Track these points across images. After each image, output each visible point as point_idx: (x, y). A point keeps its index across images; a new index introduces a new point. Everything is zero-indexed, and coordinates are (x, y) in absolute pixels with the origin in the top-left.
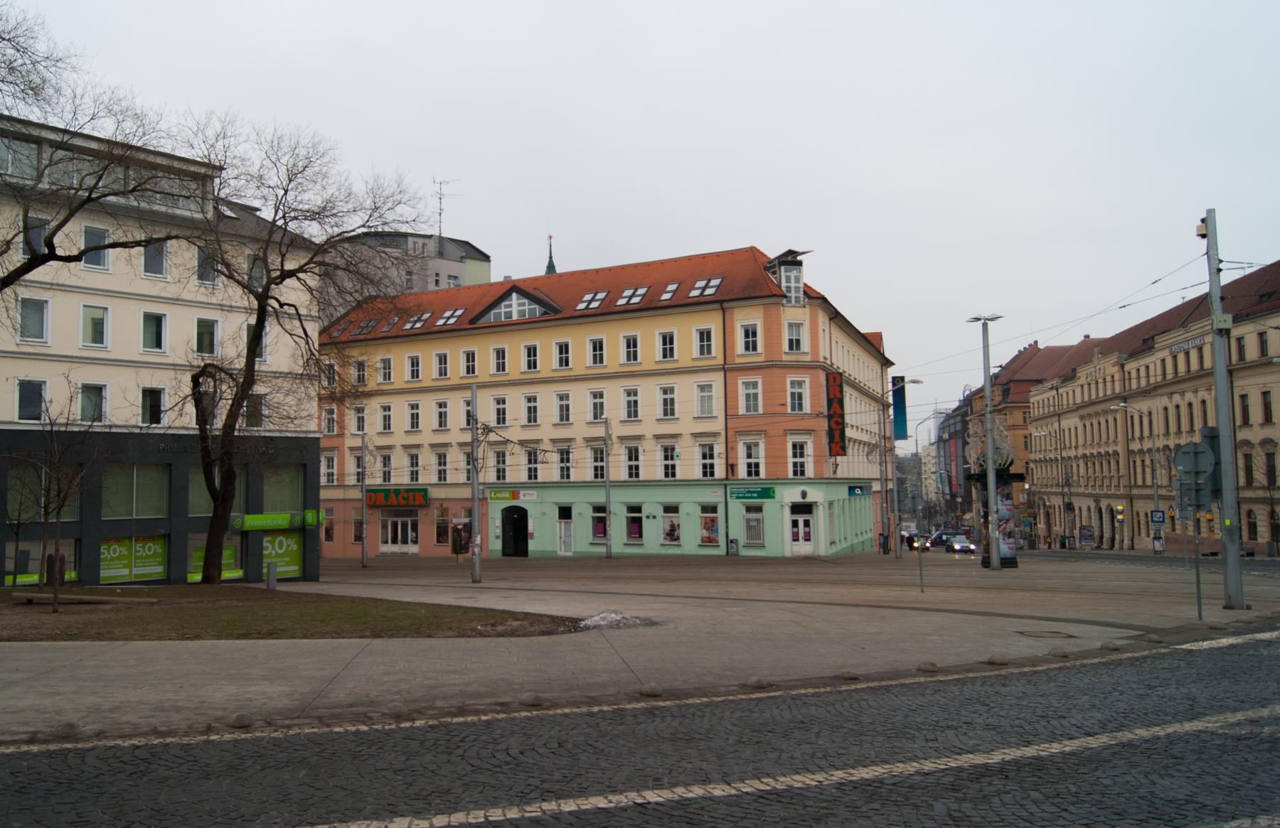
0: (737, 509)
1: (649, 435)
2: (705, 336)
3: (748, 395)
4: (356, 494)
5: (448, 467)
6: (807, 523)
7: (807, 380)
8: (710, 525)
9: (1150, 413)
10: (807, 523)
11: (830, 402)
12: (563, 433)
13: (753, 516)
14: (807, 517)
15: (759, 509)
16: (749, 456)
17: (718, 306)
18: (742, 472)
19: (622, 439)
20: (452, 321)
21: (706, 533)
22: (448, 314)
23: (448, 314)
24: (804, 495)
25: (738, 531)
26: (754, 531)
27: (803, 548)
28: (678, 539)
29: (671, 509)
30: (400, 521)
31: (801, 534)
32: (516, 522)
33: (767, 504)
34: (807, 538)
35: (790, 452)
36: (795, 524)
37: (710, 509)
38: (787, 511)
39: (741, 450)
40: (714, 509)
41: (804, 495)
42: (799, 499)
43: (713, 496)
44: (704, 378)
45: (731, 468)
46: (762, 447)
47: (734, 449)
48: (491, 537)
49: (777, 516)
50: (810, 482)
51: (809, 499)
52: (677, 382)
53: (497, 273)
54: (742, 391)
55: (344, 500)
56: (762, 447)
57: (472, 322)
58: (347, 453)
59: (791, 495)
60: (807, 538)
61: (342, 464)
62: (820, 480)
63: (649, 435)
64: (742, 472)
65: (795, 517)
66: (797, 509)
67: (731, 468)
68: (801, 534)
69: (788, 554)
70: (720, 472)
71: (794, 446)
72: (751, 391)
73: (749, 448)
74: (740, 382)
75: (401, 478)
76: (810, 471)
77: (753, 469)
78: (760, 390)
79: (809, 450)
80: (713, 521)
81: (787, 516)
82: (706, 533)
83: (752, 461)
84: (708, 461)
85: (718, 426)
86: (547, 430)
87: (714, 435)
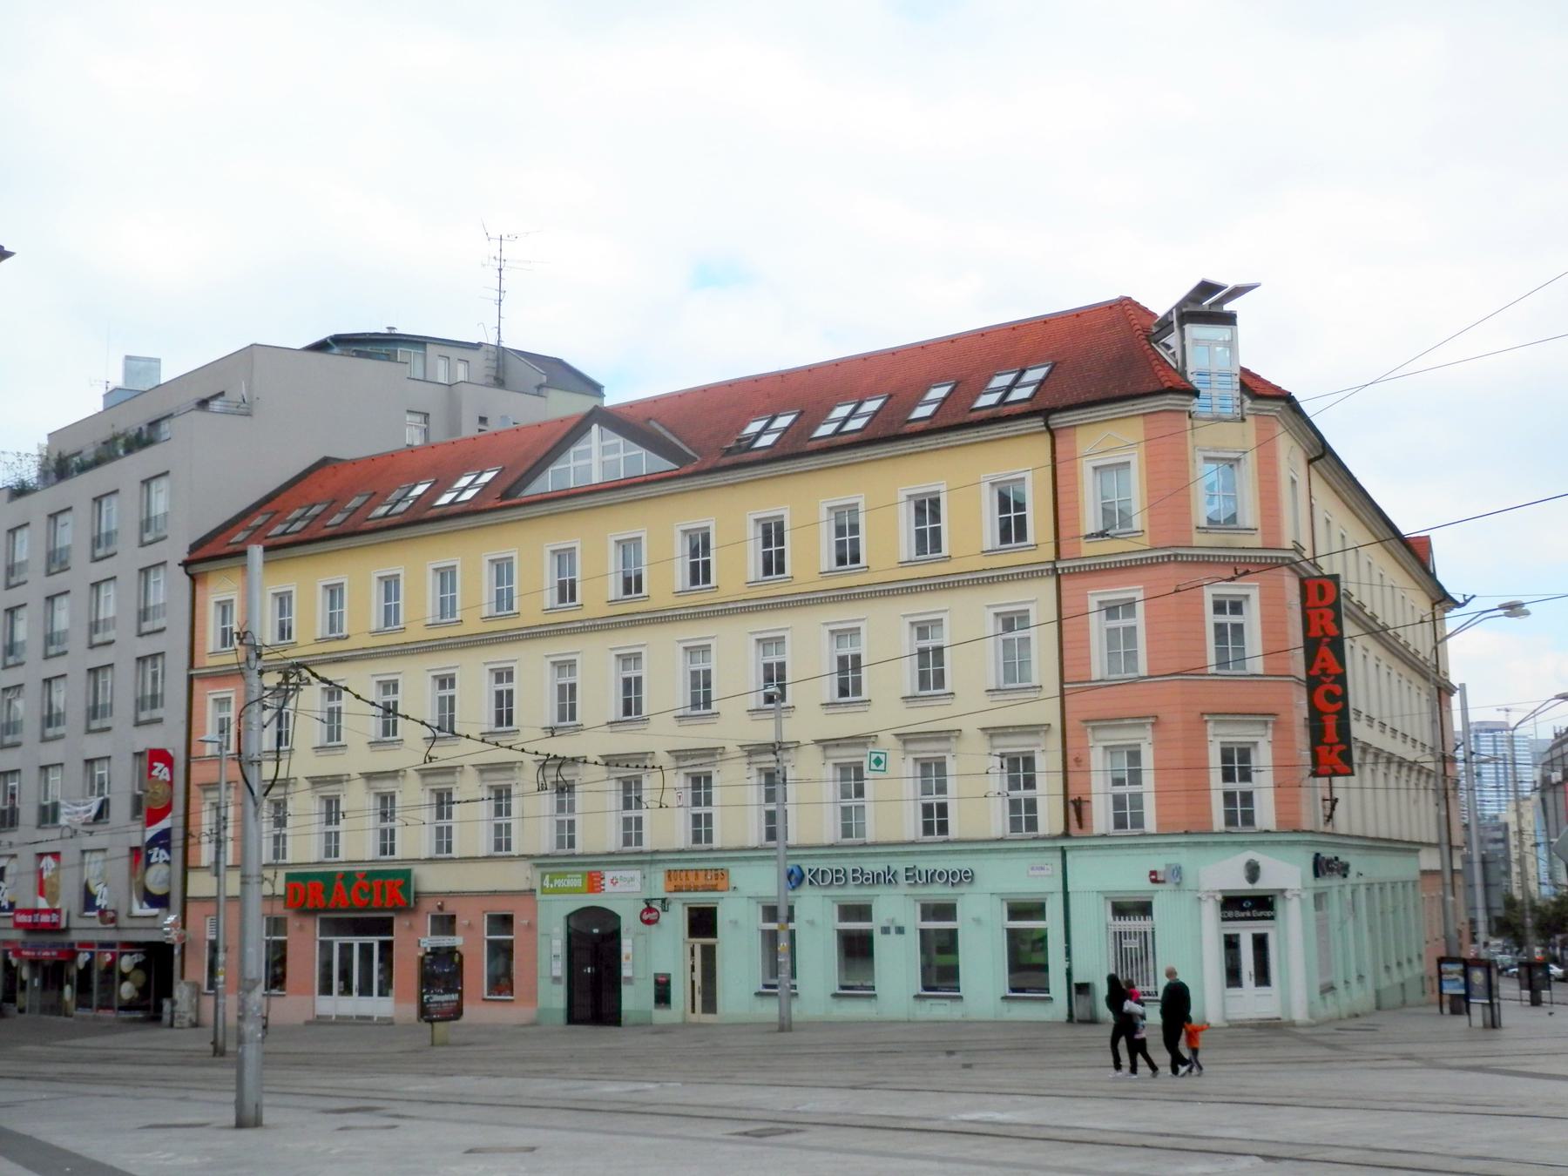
10: (1260, 943)
14: (1260, 927)
22: (464, 481)
24: (1253, 872)
36: (1231, 943)
40: (1035, 910)
41: (1253, 872)
42: (1238, 883)
44: (1010, 597)
45: (1076, 808)
50: (1267, 839)
51: (1264, 884)
57: (505, 495)
65: (1232, 928)
66: (1232, 904)
67: (1076, 808)
70: (1050, 817)
71: (1227, 756)
75: (359, 846)
76: (1265, 813)
78: (1139, 620)
79: (1263, 757)
81: (1212, 928)
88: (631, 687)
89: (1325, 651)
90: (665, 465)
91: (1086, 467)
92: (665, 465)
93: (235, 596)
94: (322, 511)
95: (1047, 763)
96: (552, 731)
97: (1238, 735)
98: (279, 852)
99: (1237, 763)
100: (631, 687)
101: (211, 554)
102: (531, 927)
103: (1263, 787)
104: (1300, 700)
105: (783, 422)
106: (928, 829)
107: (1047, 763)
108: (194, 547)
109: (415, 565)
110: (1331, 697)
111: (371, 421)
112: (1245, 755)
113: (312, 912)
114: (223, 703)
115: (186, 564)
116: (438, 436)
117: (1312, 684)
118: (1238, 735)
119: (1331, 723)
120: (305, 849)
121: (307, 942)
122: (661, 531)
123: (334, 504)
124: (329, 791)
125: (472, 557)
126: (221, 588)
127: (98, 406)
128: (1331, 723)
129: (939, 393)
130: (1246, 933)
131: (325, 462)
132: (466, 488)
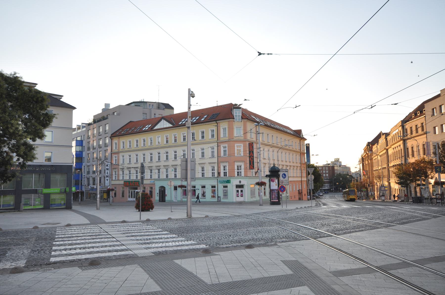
0: (221, 186)
1: (207, 163)
2: (213, 131)
3: (224, 150)
4: (122, 182)
5: (205, 172)
6: (242, 191)
7: (242, 145)
8: (213, 192)
9: (412, 147)
10: (242, 191)
11: (250, 152)
12: (158, 164)
13: (225, 189)
14: (242, 189)
15: (226, 187)
16: (224, 170)
17: (215, 122)
18: (222, 174)
19: (199, 164)
20: (195, 121)
21: (213, 195)
22: (183, 120)
23: (183, 120)
24: (240, 182)
25: (221, 194)
26: (226, 194)
27: (240, 199)
28: (205, 196)
29: (204, 187)
30: (133, 191)
31: (240, 195)
32: (162, 191)
33: (229, 185)
34: (242, 196)
35: (236, 168)
36: (238, 191)
37: (213, 187)
38: (235, 187)
39: (222, 168)
40: (214, 187)
41: (240, 182)
42: (238, 184)
43: (214, 183)
44: (211, 145)
45: (219, 173)
46: (227, 167)
47: (220, 167)
48: (156, 197)
49: (232, 188)
50: (243, 178)
51: (242, 183)
52: (169, 150)
53: (176, 112)
54: (222, 149)
55: (119, 184)
56: (227, 167)
57: (151, 129)
58: (120, 170)
59: (235, 182)
60: (242, 196)
61: (118, 173)
62: (246, 176)
63: (207, 163)
64: (222, 174)
65: (238, 189)
66: (237, 186)
67: (219, 173)
68: (240, 195)
69: (234, 201)
70: (216, 175)
71: (238, 167)
72: (225, 149)
73: (224, 167)
74: (236, 145)
75: (133, 178)
76: (243, 174)
77: (225, 174)
78: (227, 149)
79: (243, 167)
80: (215, 190)
81: (235, 189)
82: (213, 195)
83: (225, 171)
84: (213, 172)
85: (215, 160)
86: (154, 164)
87: (214, 163)
88: (203, 153)
89: (251, 153)
90: (171, 125)
91: (221, 128)
92: (171, 125)
93: (117, 142)
94: (130, 129)
95: (216, 168)
96: (157, 162)
97: (239, 164)
98: (123, 178)
99: (239, 168)
100: (203, 153)
101: (113, 136)
102: (155, 189)
103: (243, 171)
104: (248, 159)
105: (197, 118)
106: (224, 175)
107: (216, 168)
108: (111, 135)
109: (140, 138)
110: (252, 159)
111: (137, 116)
112: (240, 166)
113: (127, 186)
114: (116, 157)
115: (110, 137)
116: (148, 118)
117: (250, 157)
118: (239, 164)
119: (252, 162)
120: (127, 178)
121: (127, 190)
122: (171, 134)
123: (130, 129)
124: (203, 165)
125: (148, 137)
126: (115, 141)
127: (101, 112)
128: (252, 162)
129: (205, 117)
130: (240, 190)
131: (131, 122)
132: (147, 128)
